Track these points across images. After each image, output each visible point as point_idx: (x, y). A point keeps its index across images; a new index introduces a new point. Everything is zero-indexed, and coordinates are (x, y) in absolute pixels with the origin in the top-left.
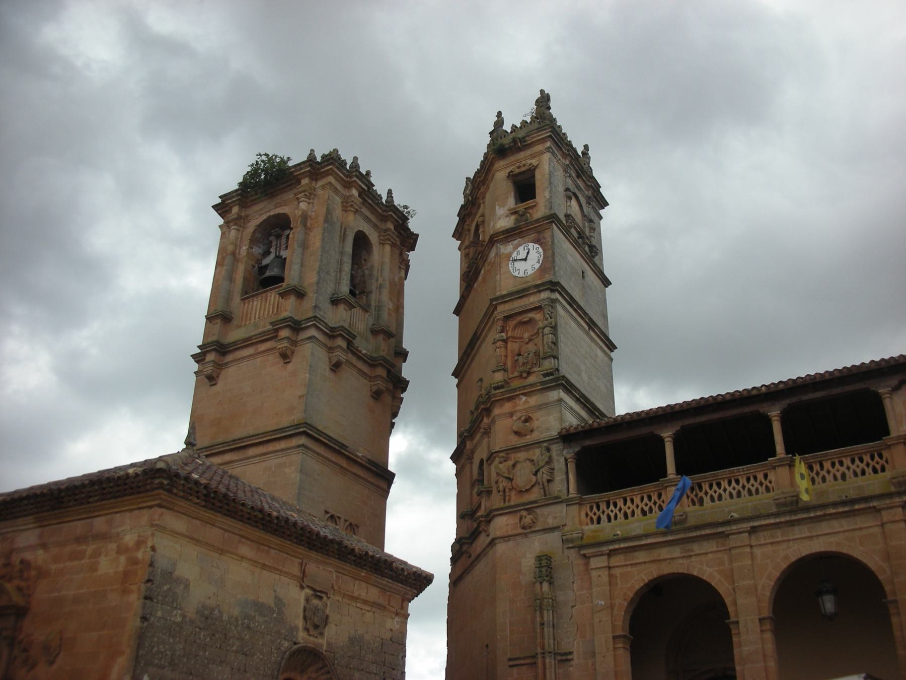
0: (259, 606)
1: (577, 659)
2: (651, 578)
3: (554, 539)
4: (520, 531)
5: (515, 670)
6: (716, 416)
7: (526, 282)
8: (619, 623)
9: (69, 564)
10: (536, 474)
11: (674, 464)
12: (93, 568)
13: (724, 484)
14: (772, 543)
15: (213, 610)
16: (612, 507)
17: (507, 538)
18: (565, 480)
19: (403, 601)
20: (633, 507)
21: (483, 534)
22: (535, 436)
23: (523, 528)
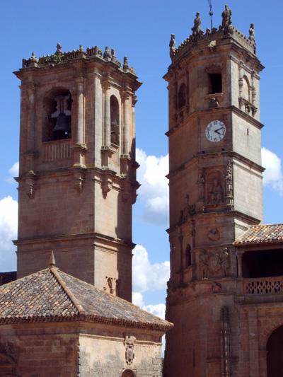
3: (230, 299)
5: (210, 364)
9: (35, 347)
10: (220, 264)
12: (49, 350)
16: (260, 285)
18: (236, 267)
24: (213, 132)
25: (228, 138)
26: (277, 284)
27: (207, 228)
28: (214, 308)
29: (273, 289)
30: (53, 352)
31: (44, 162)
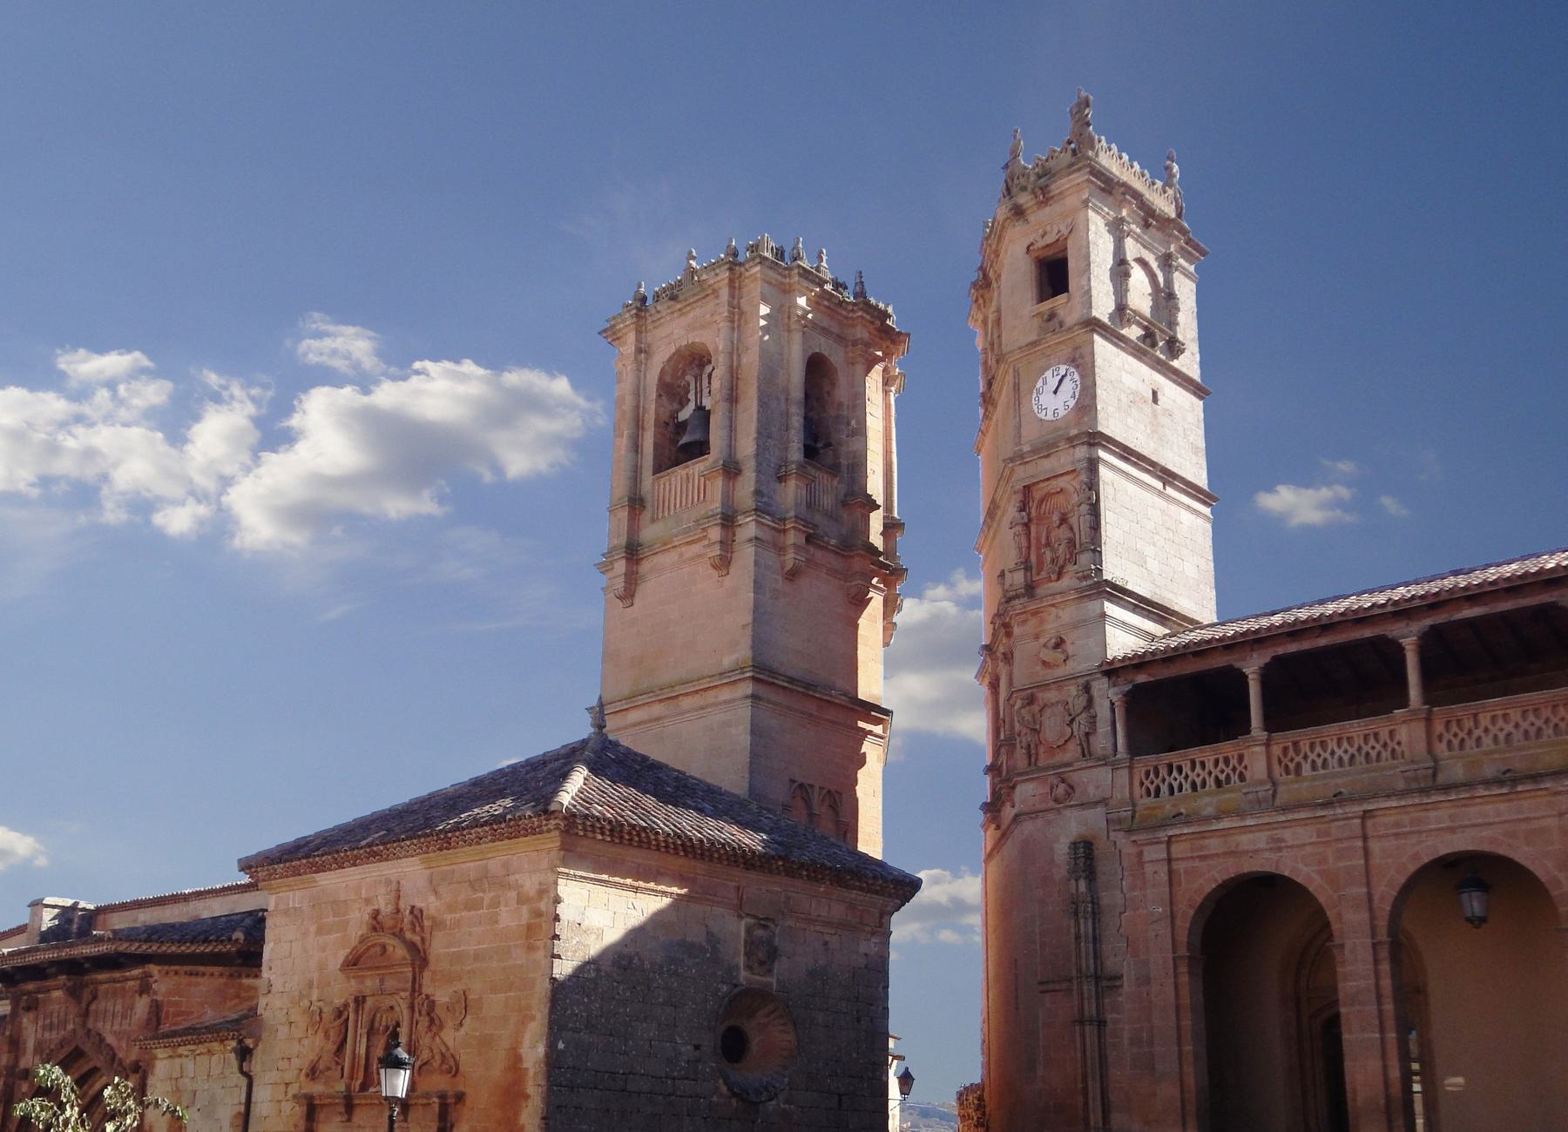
0: (689, 948)
1: (1127, 986)
2: (1226, 877)
3: (1096, 817)
4: (1052, 804)
6: (1323, 642)
7: (1056, 430)
8: (1183, 937)
11: (1261, 712)
13: (1332, 745)
14: (1396, 835)
15: (631, 959)
16: (1175, 773)
17: (1032, 814)
18: (1110, 733)
19: (881, 916)
20: (1204, 774)
21: (1008, 804)
22: (1073, 667)
23: (1056, 800)
24: (1052, 400)
25: (1086, 403)
26: (1221, 765)
27: (1037, 637)
28: (1056, 846)
29: (1211, 782)
31: (653, 520)
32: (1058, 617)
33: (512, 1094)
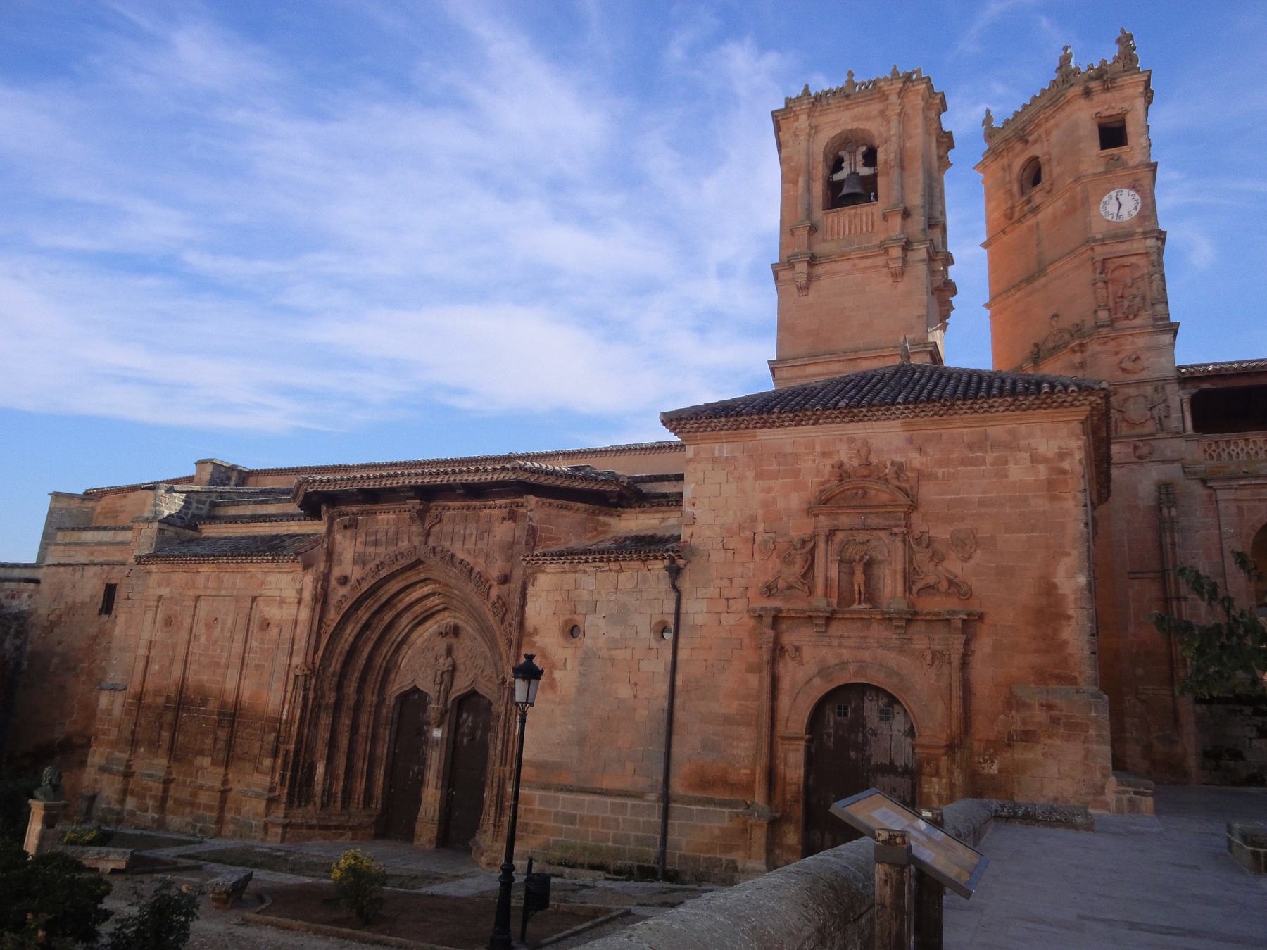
4: (1135, 459)
5: (1136, 582)
22: (1144, 375)
27: (1117, 353)
30: (1011, 479)
31: (825, 241)
32: (1133, 343)
33: (1048, 612)
